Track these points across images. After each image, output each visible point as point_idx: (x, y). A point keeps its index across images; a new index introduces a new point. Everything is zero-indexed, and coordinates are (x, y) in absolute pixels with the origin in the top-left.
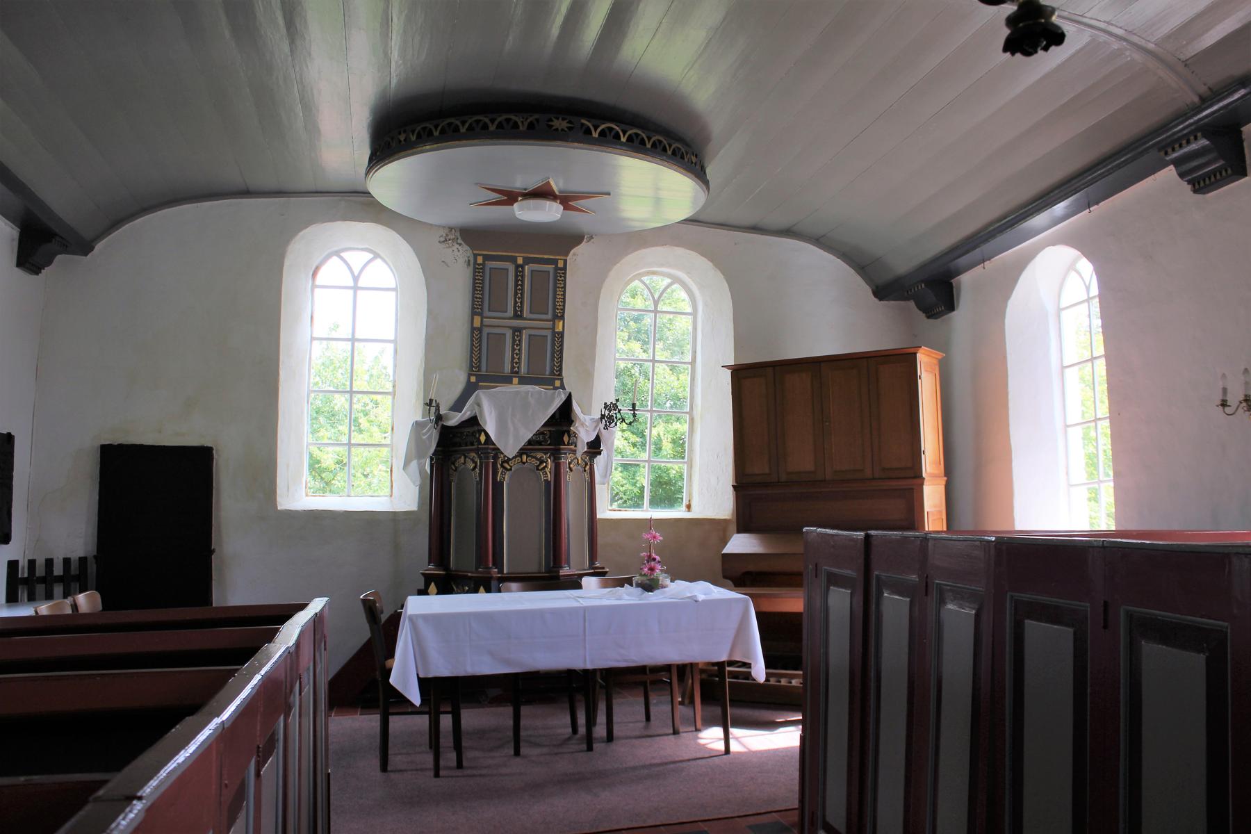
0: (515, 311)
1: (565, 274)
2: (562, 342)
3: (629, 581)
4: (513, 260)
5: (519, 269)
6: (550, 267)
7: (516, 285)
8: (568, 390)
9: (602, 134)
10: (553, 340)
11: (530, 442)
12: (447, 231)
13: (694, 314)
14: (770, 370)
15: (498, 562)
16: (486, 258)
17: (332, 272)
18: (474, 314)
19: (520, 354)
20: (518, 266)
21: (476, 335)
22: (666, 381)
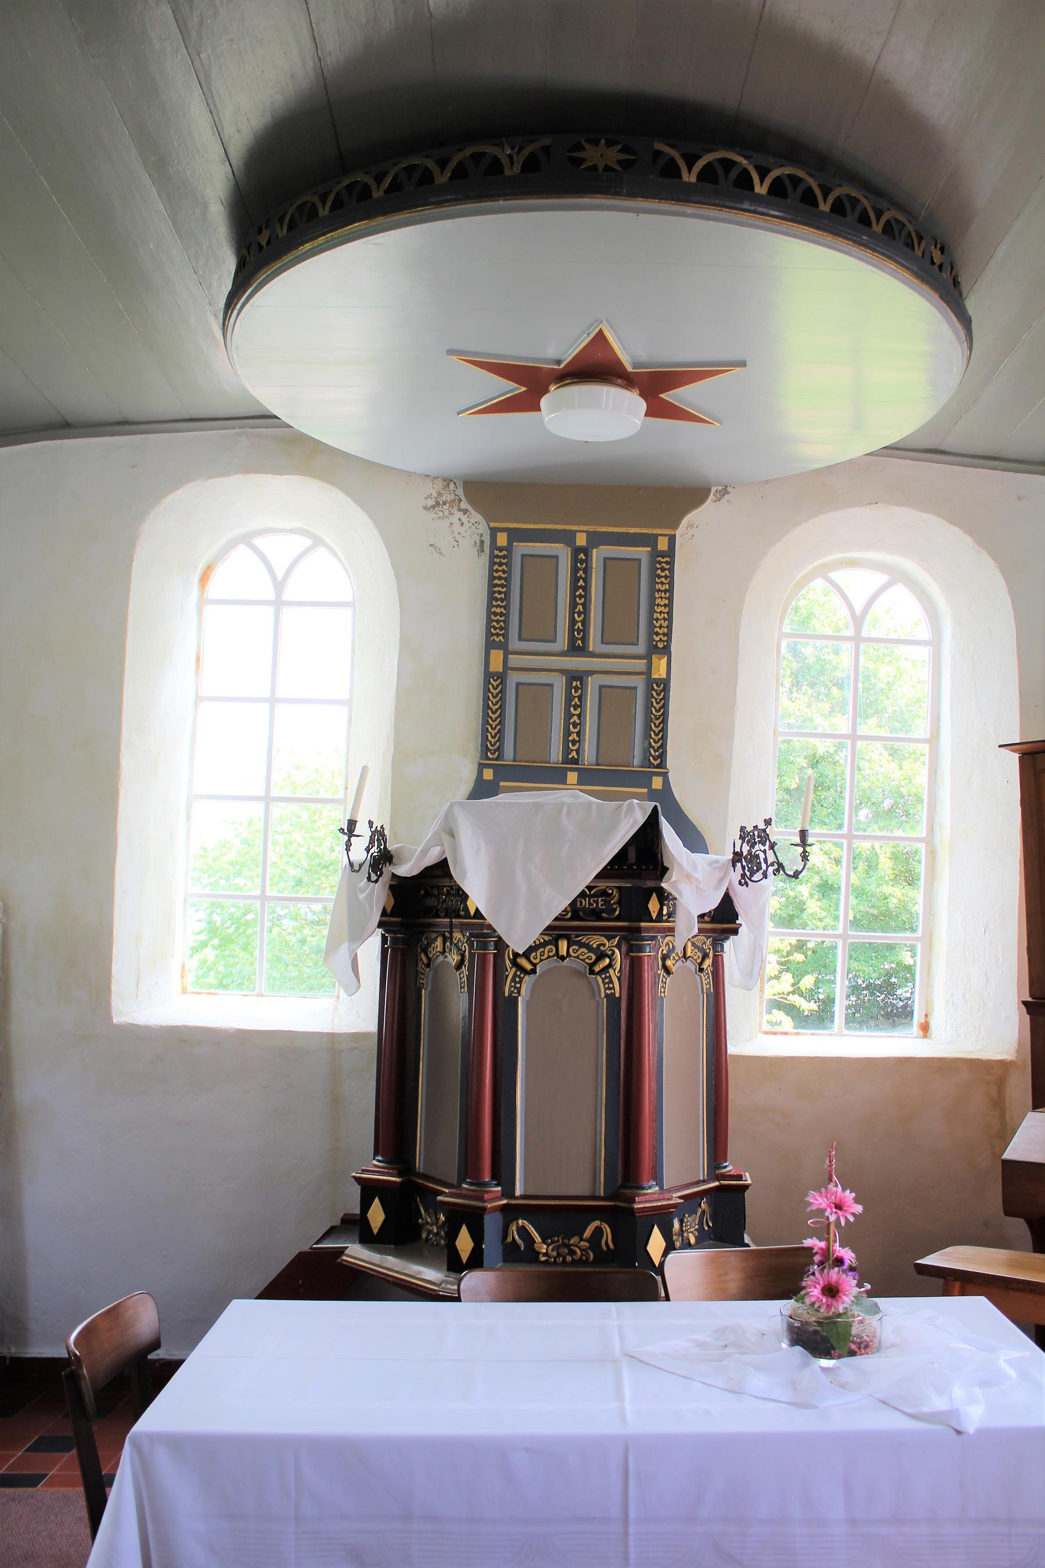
0: (572, 639)
1: (671, 563)
2: (666, 698)
4: (567, 538)
5: (580, 558)
6: (641, 552)
7: (574, 587)
9: (708, 175)
10: (649, 697)
11: (575, 910)
12: (439, 485)
15: (503, 1172)
16: (515, 536)
17: (239, 574)
18: (490, 645)
19: (580, 724)
20: (577, 551)
21: (494, 684)
22: (879, 769)
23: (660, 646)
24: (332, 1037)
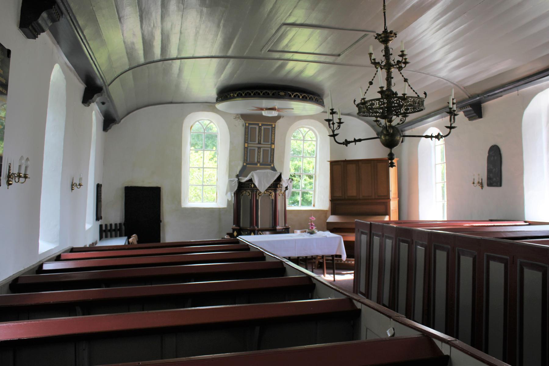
3: (305, 231)
6: (270, 127)
8: (279, 170)
11: (269, 187)
13: (316, 141)
14: (342, 163)
15: (257, 225)
18: (245, 142)
20: (259, 127)
21: (246, 149)
23: (273, 143)
24: (219, 208)
